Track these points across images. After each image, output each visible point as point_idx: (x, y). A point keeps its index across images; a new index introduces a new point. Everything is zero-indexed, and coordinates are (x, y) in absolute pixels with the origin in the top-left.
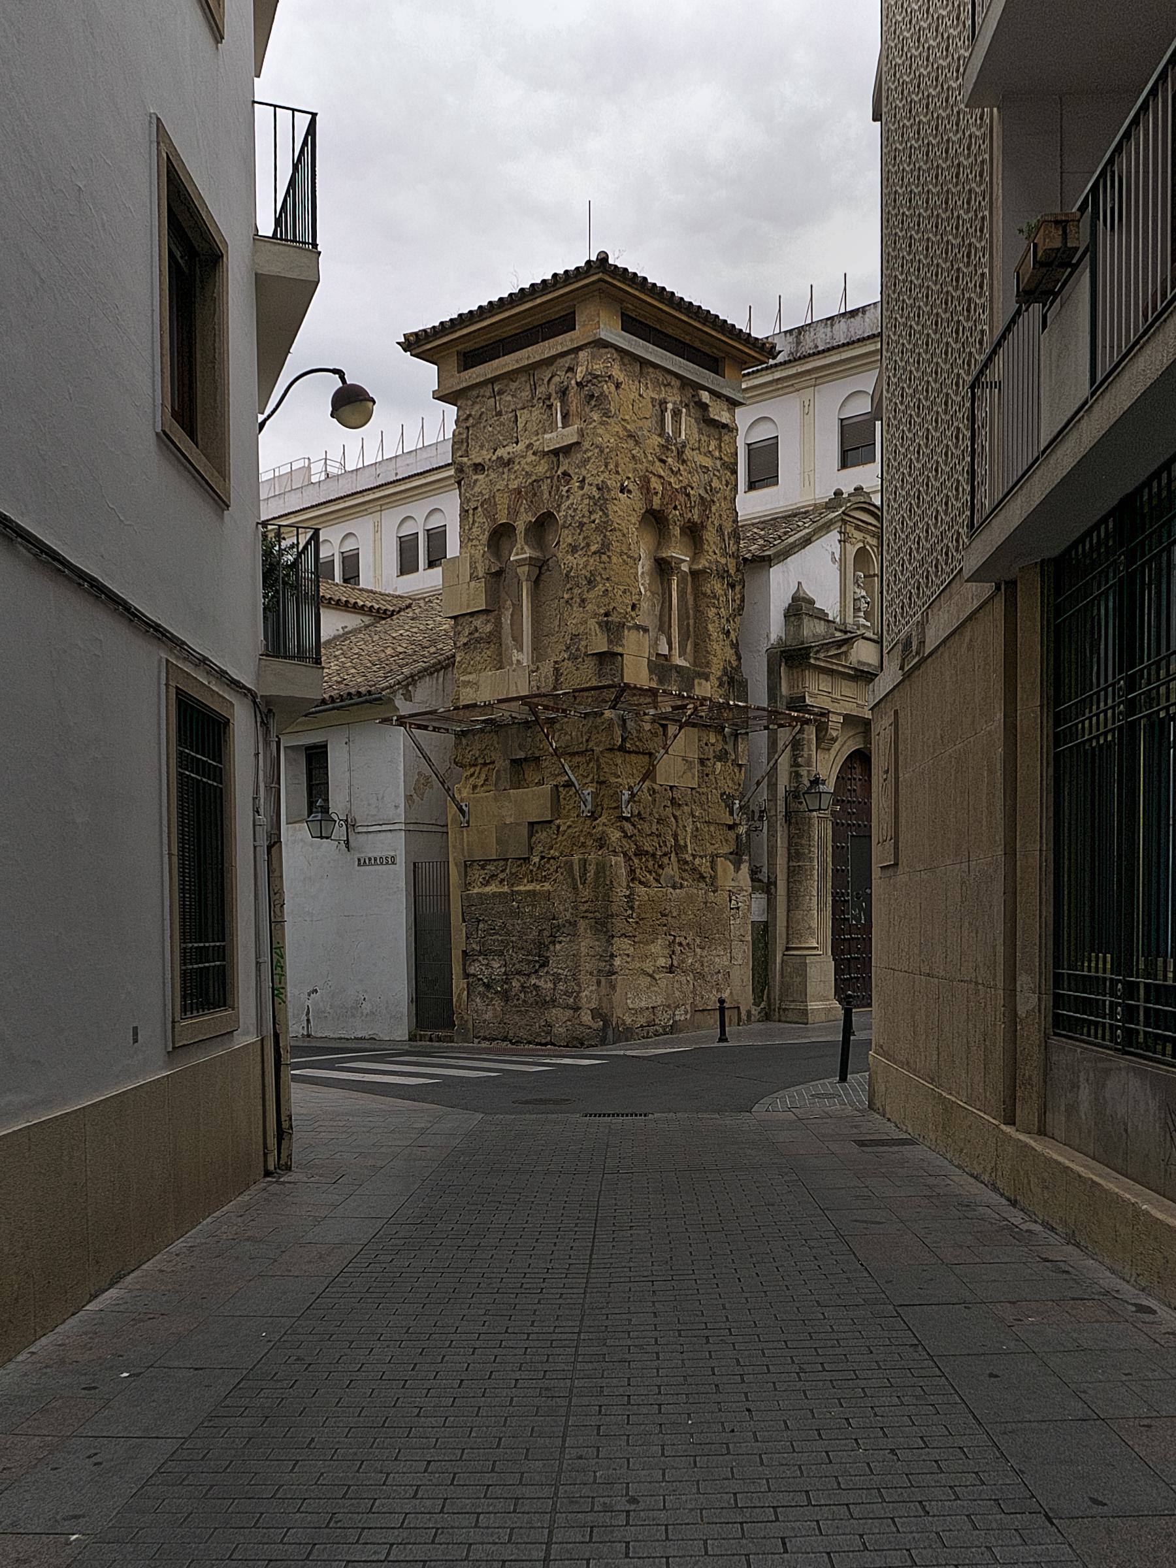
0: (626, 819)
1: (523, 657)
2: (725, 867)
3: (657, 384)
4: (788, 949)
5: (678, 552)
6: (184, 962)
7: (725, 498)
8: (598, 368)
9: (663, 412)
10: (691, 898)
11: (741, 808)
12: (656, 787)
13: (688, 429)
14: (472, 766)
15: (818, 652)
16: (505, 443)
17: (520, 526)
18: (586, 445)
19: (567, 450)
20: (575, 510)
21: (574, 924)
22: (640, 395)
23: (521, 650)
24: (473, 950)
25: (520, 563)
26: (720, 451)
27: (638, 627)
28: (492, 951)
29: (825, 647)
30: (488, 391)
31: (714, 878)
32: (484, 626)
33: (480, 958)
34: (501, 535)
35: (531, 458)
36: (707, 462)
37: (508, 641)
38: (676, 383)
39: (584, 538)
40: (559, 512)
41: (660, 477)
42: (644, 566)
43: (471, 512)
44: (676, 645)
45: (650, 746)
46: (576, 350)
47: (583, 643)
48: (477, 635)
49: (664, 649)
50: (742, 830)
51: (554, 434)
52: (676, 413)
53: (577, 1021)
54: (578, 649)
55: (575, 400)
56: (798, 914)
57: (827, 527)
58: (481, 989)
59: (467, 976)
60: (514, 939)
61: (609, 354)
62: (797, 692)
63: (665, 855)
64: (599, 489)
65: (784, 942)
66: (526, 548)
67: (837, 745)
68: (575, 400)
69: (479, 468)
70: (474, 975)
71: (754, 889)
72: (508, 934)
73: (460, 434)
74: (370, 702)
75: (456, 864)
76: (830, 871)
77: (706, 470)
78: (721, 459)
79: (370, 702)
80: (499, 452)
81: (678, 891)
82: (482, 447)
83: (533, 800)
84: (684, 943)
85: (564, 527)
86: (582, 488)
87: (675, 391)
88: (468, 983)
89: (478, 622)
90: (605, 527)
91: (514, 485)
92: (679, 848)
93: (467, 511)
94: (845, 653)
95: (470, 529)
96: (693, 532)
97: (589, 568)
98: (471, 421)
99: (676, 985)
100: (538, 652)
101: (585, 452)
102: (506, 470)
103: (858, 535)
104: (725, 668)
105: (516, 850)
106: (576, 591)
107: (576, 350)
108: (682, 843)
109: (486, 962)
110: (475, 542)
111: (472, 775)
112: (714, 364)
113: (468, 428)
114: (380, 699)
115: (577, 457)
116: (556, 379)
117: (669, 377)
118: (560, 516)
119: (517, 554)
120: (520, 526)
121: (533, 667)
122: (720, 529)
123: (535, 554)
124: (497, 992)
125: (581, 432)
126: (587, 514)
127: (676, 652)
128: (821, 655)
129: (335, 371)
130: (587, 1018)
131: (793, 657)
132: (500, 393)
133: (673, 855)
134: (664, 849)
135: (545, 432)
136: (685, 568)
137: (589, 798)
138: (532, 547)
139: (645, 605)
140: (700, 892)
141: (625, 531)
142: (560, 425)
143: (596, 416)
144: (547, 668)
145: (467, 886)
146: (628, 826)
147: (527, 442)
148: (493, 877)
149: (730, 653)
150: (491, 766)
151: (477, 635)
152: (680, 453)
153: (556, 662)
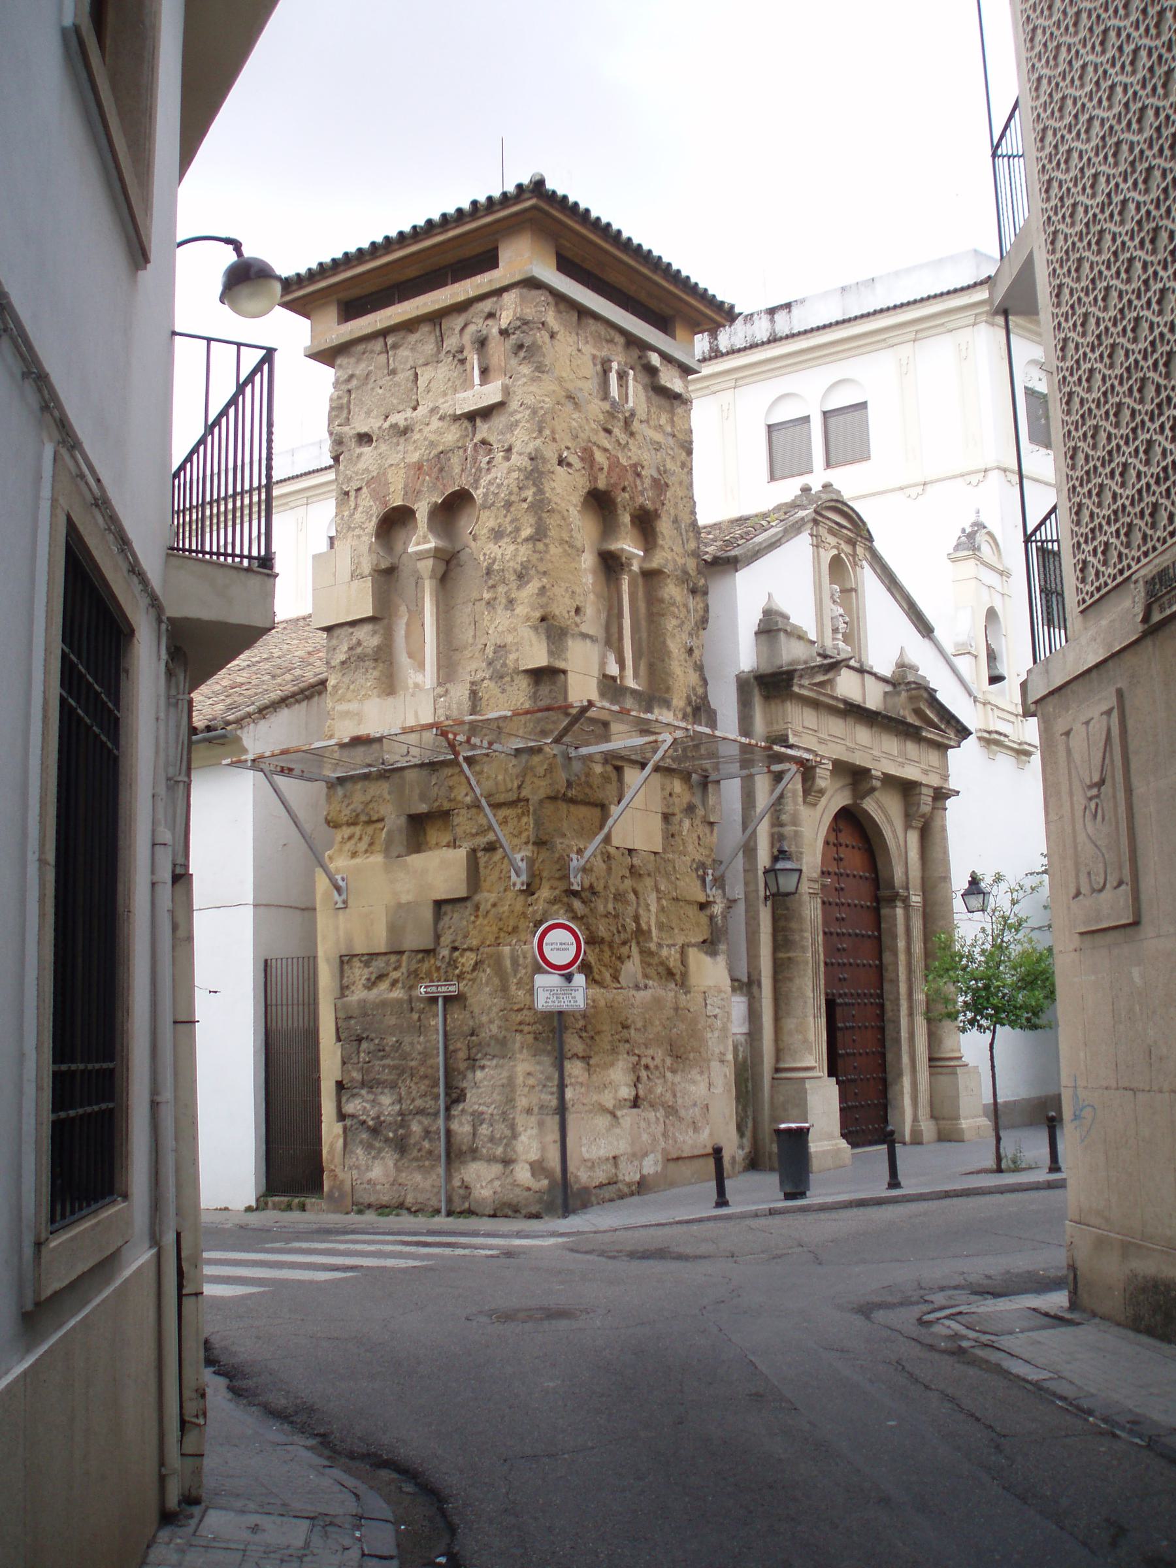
0: (575, 894)
1: (428, 677)
2: (696, 957)
3: (598, 338)
4: (777, 1070)
5: (628, 545)
6: (59, 1103)
7: (681, 483)
8: (530, 312)
9: (606, 372)
10: (658, 1002)
11: (715, 880)
12: (612, 850)
13: (636, 395)
14: (349, 824)
15: (801, 677)
16: (400, 408)
17: (422, 511)
18: (514, 405)
19: (486, 413)
20: (499, 486)
21: (503, 1043)
22: (579, 350)
23: (421, 666)
24: (352, 1080)
25: (421, 556)
26: (673, 426)
27: (585, 636)
28: (379, 1083)
29: (812, 670)
30: (378, 345)
31: (685, 975)
32: (368, 638)
33: (363, 1092)
34: (394, 522)
35: (435, 424)
36: (658, 437)
37: (403, 659)
38: (620, 340)
39: (512, 521)
40: (477, 488)
41: (606, 450)
42: (588, 560)
43: (352, 494)
44: (629, 663)
45: (600, 795)
46: (499, 292)
47: (512, 657)
48: (359, 650)
49: (613, 669)
50: (717, 909)
51: (469, 393)
52: (622, 376)
53: (509, 1180)
54: (504, 665)
55: (498, 350)
56: (790, 1024)
57: (795, 529)
58: (364, 1136)
59: (342, 1116)
60: (413, 1063)
61: (542, 296)
62: (778, 728)
63: (624, 943)
64: (532, 459)
65: (773, 1061)
66: (430, 536)
67: (824, 801)
68: (498, 350)
69: (365, 438)
70: (353, 1116)
71: (734, 990)
72: (404, 1057)
73: (339, 398)
74: (209, 740)
75: (328, 960)
76: (822, 965)
77: (658, 447)
78: (674, 436)
79: (209, 740)
80: (393, 419)
81: (642, 993)
82: (368, 413)
83: (440, 869)
84: (652, 1065)
85: (484, 507)
86: (508, 459)
87: (620, 349)
88: (345, 1129)
89: (362, 633)
90: (540, 507)
91: (414, 457)
92: (641, 934)
93: (347, 493)
94: (830, 681)
95: (351, 515)
96: (645, 523)
97: (519, 559)
98: (354, 382)
99: (643, 1125)
100: (447, 669)
101: (512, 414)
102: (402, 440)
103: (832, 540)
104: (688, 697)
105: (417, 938)
106: (501, 589)
107: (499, 292)
108: (644, 927)
109: (371, 1097)
110: (357, 532)
111: (350, 838)
112: (663, 323)
113: (349, 391)
114: (224, 736)
115: (499, 421)
116: (472, 329)
117: (612, 332)
118: (478, 494)
119: (418, 544)
120: (422, 511)
121: (440, 690)
122: (676, 521)
123: (441, 544)
124: (387, 1140)
125: (506, 391)
126: (516, 490)
127: (629, 671)
128: (806, 682)
129: (228, 241)
130: (523, 1174)
131: (772, 685)
132: (395, 346)
133: (634, 944)
134: (623, 936)
135: (455, 391)
136: (635, 567)
137: (523, 865)
138: (437, 535)
139: (589, 611)
140: (669, 993)
141: (566, 513)
142: (477, 380)
143: (526, 370)
144: (460, 692)
145: (344, 989)
146: (577, 904)
147: (431, 405)
148: (381, 977)
149: (693, 678)
150: (380, 825)
151: (359, 650)
152: (627, 423)
153: (472, 683)
